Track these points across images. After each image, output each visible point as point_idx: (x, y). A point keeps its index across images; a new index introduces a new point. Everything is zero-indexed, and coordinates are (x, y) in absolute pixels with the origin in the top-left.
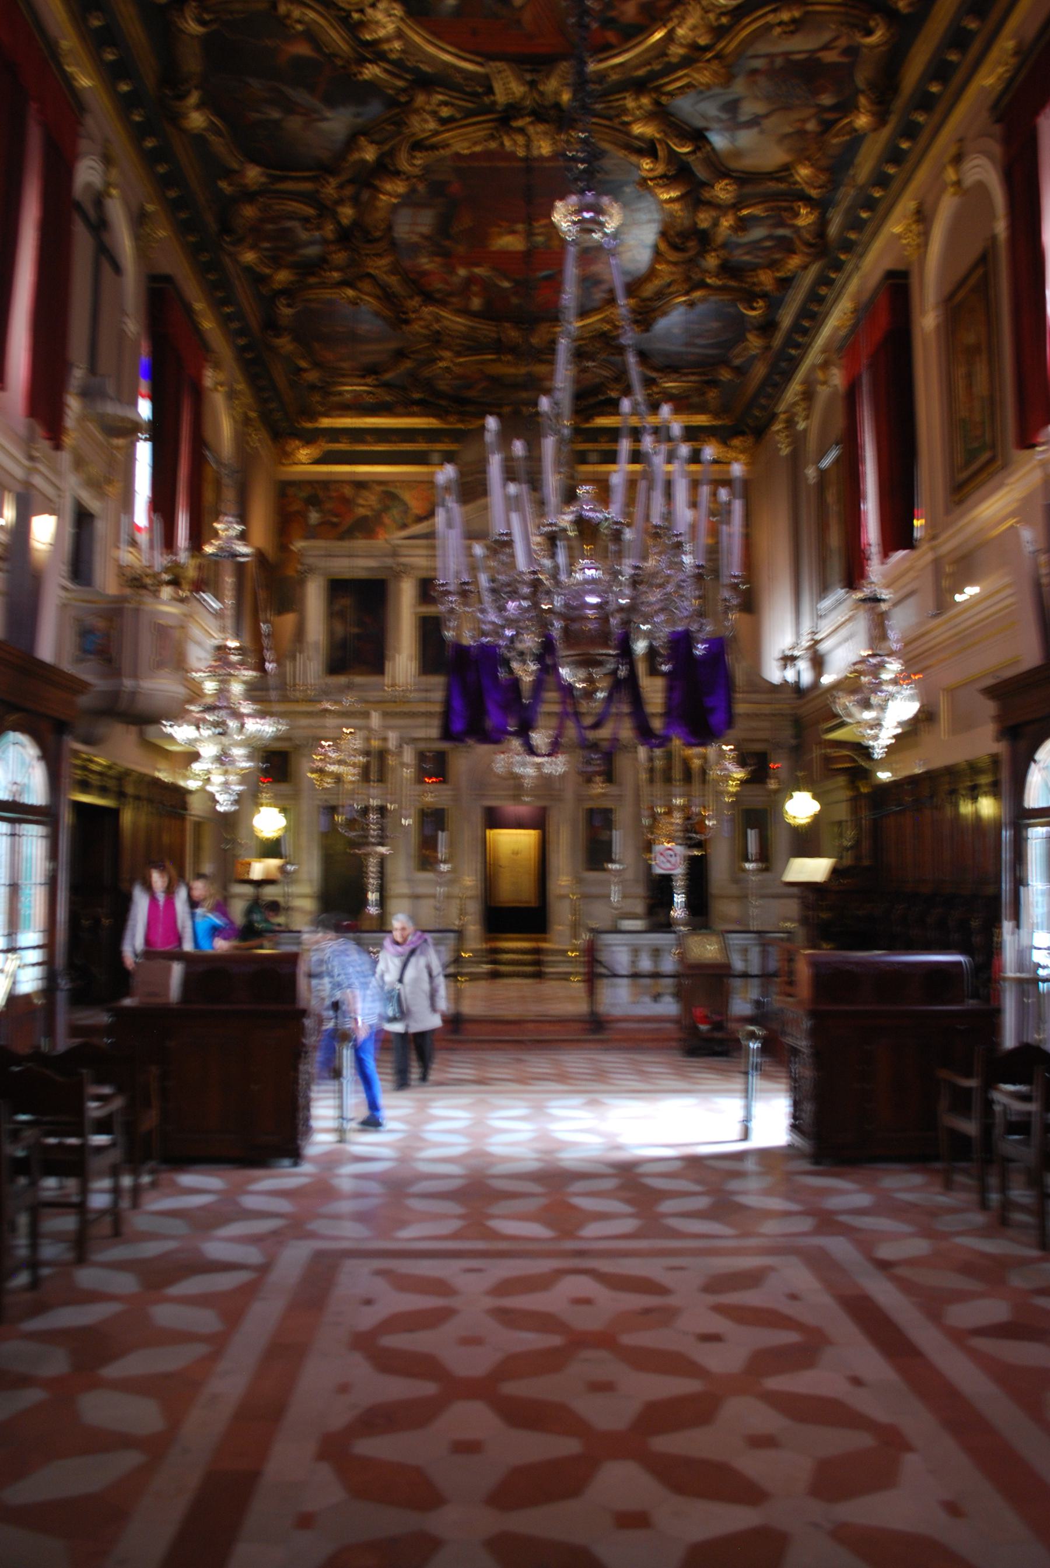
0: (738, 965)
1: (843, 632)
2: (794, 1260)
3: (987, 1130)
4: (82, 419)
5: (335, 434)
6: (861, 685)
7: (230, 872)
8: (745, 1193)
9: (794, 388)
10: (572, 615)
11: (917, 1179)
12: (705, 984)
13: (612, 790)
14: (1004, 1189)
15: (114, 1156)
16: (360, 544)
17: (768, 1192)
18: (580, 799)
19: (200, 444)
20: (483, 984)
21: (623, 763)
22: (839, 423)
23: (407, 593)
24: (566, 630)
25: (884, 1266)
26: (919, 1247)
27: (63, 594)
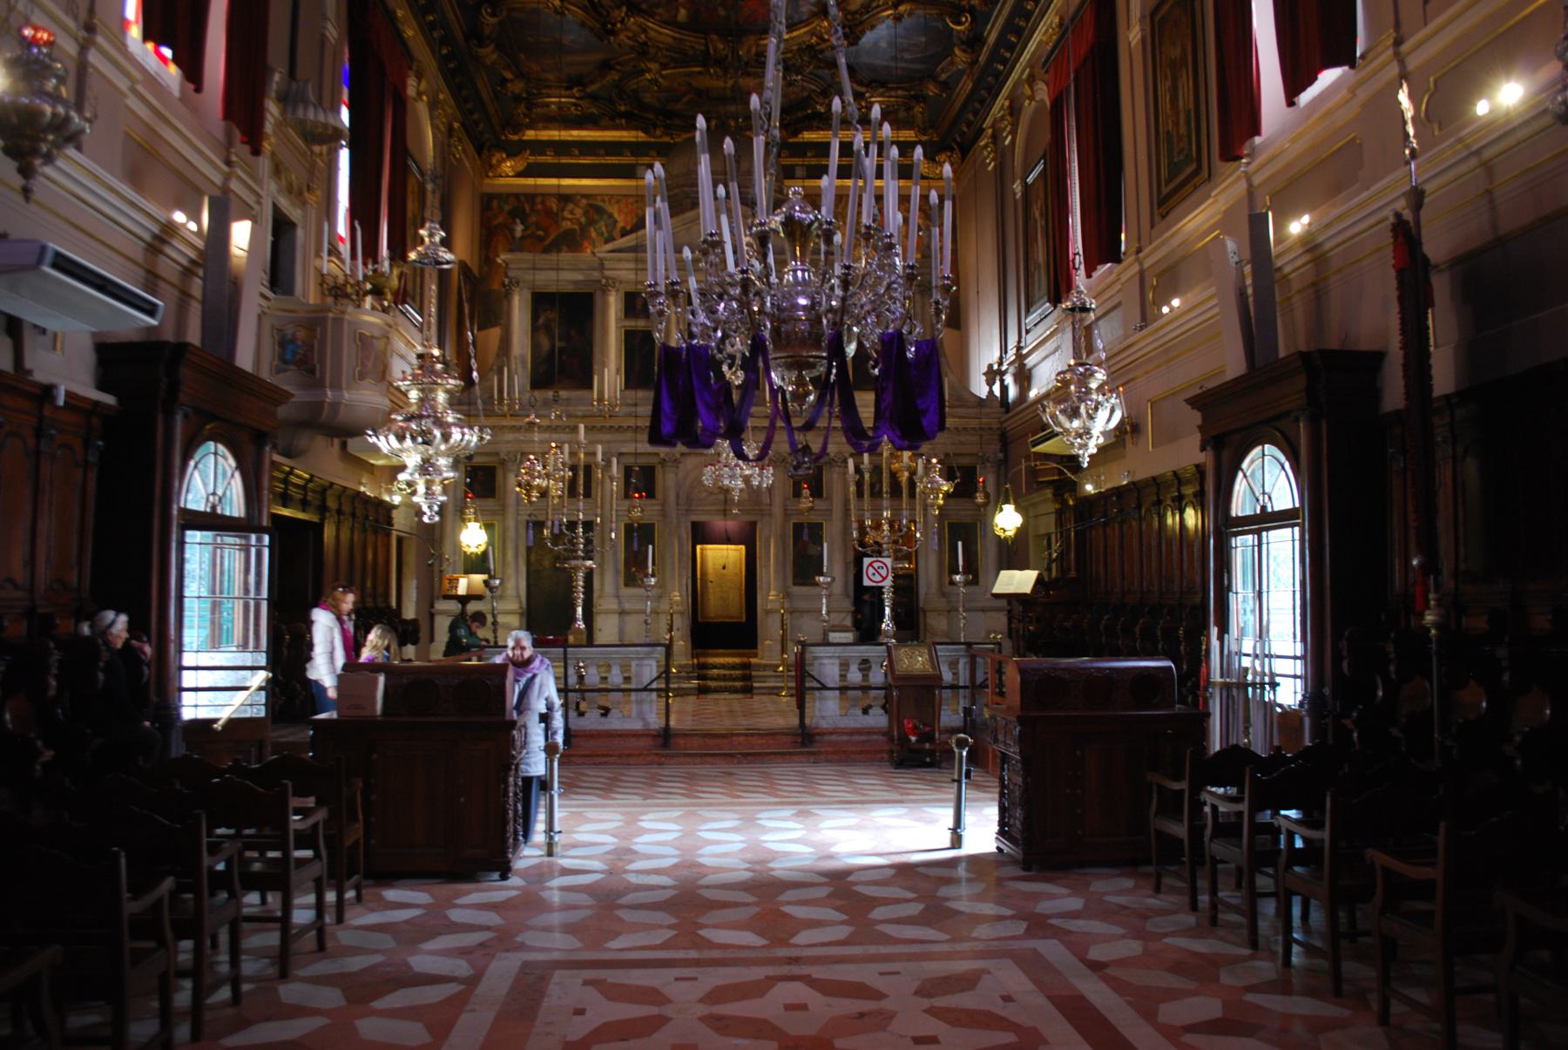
0: (947, 676)
1: (1050, 346)
2: (1009, 962)
3: (1196, 831)
4: (279, 125)
5: (540, 147)
6: (1070, 394)
7: (436, 586)
8: (958, 898)
9: (1001, 101)
10: (783, 316)
11: (1129, 883)
12: (913, 696)
13: (820, 504)
14: (1214, 891)
15: (318, 869)
16: (566, 257)
17: (979, 898)
18: (787, 514)
19: (402, 154)
20: (692, 699)
21: (831, 478)
22: (1046, 137)
23: (613, 306)
24: (776, 331)
25: (1097, 967)
26: (1133, 948)
27: (264, 303)
